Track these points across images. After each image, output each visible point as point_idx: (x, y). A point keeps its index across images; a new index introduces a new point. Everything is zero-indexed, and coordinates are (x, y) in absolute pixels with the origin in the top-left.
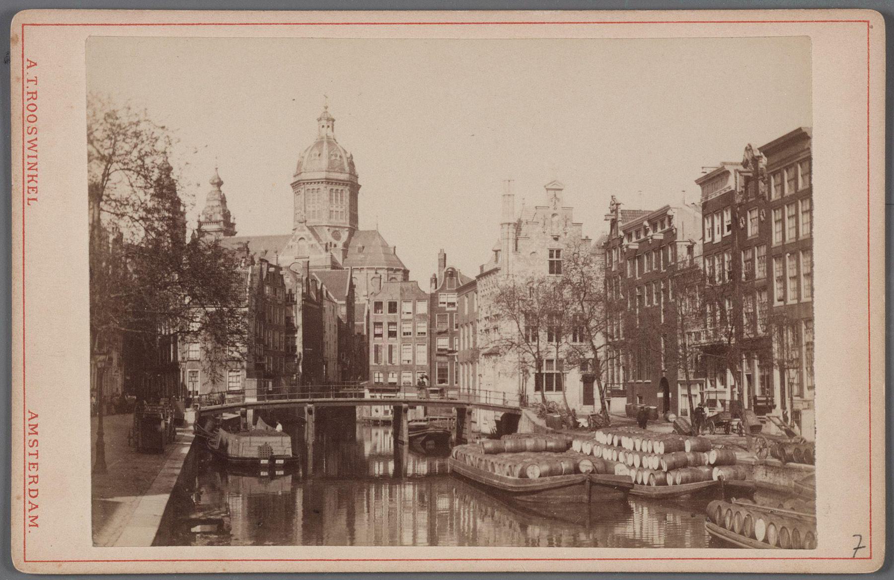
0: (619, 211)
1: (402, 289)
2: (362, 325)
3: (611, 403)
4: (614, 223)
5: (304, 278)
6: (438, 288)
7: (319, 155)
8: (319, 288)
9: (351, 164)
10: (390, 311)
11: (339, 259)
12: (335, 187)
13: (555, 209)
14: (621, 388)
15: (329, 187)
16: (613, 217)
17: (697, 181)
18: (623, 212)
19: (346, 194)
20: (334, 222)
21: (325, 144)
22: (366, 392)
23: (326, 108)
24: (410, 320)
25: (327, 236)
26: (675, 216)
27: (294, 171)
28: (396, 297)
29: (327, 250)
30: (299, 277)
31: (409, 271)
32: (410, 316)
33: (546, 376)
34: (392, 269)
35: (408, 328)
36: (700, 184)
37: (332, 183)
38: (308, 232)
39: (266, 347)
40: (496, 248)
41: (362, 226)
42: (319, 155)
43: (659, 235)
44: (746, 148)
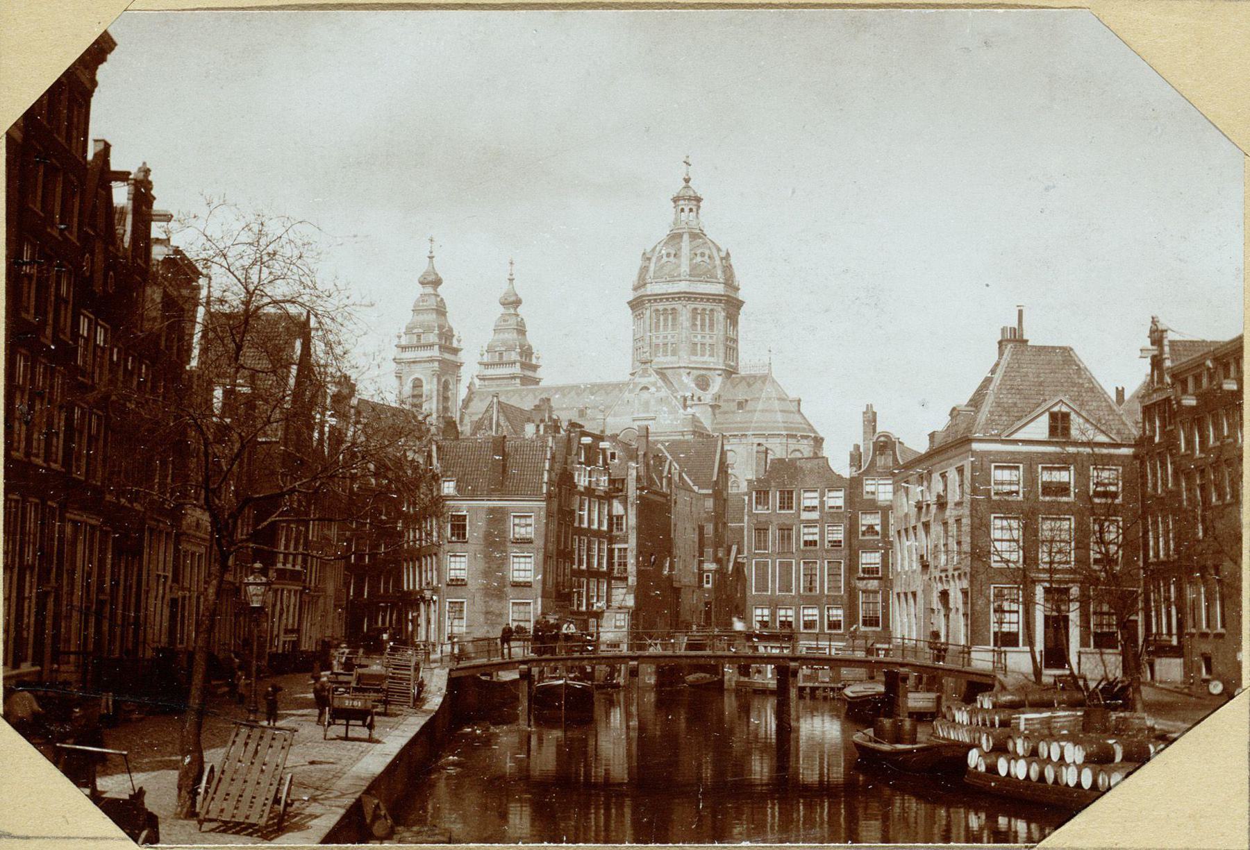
0: (1166, 342)
2: (742, 529)
4: (1157, 363)
5: (641, 453)
9: (728, 269)
12: (700, 306)
14: (1175, 642)
16: (1156, 353)
18: (1172, 343)
19: (720, 315)
20: (698, 360)
21: (686, 237)
23: (687, 181)
24: (816, 521)
27: (634, 278)
31: (822, 439)
32: (815, 515)
34: (794, 436)
35: (812, 534)
38: (654, 378)
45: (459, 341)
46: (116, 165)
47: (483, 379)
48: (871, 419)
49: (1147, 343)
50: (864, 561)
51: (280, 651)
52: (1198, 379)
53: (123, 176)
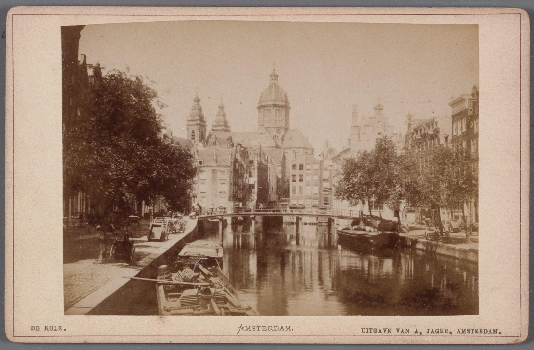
0: (412, 120)
1: (306, 158)
3: (407, 216)
4: (409, 125)
5: (259, 153)
6: (325, 157)
7: (270, 93)
8: (266, 158)
10: (300, 169)
11: (280, 143)
13: (379, 119)
15: (275, 109)
16: (409, 123)
17: (449, 104)
22: (288, 209)
23: (274, 70)
25: (275, 133)
26: (439, 122)
28: (303, 163)
29: (274, 139)
30: (256, 152)
31: (314, 149)
33: (374, 202)
36: (451, 106)
37: (270, 106)
38: (264, 130)
39: (239, 186)
40: (349, 139)
41: (292, 126)
42: (270, 93)
43: (431, 132)
44: (473, 87)
45: (206, 119)
46: (88, 62)
47: (213, 130)
48: (327, 144)
49: (407, 120)
50: (324, 185)
51: (148, 212)
52: (421, 130)
53: (91, 66)
